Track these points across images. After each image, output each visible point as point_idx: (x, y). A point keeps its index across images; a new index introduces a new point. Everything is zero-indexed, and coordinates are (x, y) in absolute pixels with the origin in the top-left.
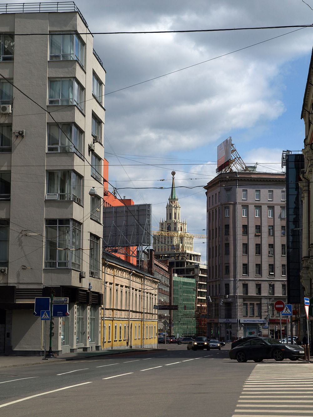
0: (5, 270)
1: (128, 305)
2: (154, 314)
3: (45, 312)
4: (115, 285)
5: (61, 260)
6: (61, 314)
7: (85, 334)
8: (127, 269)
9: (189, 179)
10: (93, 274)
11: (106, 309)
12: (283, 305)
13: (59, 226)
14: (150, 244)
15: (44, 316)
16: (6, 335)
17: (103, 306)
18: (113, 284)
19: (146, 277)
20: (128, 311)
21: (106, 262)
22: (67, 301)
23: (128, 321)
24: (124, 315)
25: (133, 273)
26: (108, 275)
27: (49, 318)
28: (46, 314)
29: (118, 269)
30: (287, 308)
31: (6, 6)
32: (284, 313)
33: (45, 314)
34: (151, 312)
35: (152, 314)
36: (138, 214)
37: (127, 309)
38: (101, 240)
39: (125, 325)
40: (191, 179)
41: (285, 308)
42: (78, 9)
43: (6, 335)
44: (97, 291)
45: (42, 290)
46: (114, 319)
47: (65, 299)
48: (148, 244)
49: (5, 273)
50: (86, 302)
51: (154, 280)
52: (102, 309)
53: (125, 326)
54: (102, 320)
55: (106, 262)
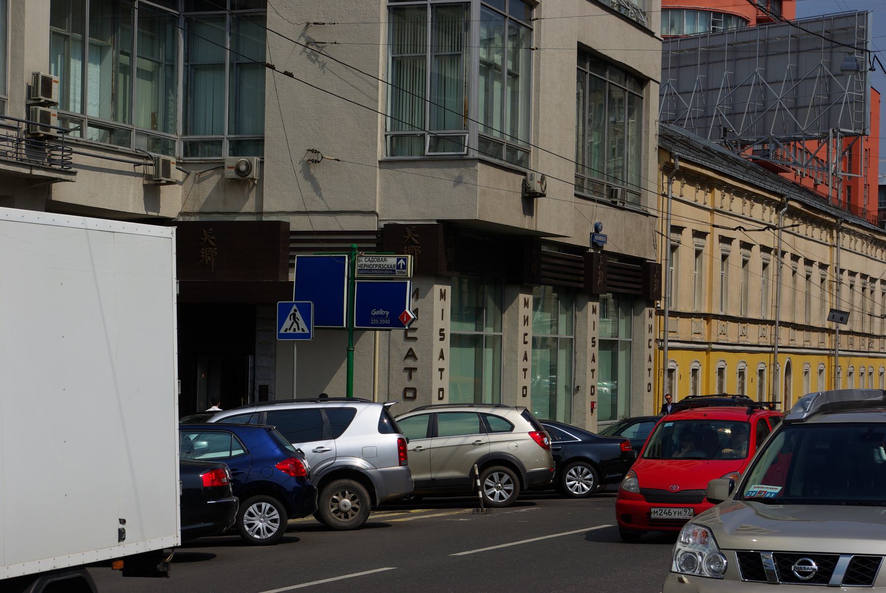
0: (249, 166)
1: (774, 304)
2: (878, 337)
3: (295, 307)
4: (716, 239)
7: (578, 395)
8: (767, 195)
10: (616, 197)
11: (674, 314)
14: (864, 130)
15: (288, 323)
16: (257, 394)
17: (661, 304)
18: (708, 237)
19: (843, 225)
20: (772, 323)
21: (673, 161)
22: (405, 267)
23: (772, 355)
24: (753, 334)
25: (790, 206)
26: (689, 207)
27: (307, 331)
28: (298, 315)
29: (729, 189)
32: (286, 330)
33: (294, 315)
34: (867, 331)
35: (871, 336)
37: (769, 318)
38: (654, 90)
39: (762, 366)
44: (633, 253)
45: (374, 237)
46: (714, 346)
47: (398, 260)
48: (858, 131)
49: (250, 176)
50: (640, 293)
51: (877, 236)
52: (660, 313)
53: (761, 372)
54: (661, 348)
55: (673, 161)
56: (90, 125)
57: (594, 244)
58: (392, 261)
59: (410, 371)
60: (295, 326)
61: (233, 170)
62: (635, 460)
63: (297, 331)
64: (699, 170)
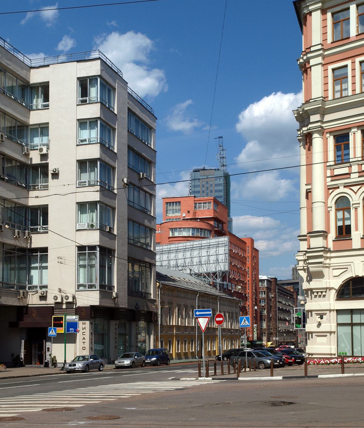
3: (53, 329)
5: (92, 282)
6: (73, 330)
9: (62, 185)
12: (222, 318)
13: (89, 253)
15: (51, 332)
16: (47, 350)
28: (53, 330)
30: (245, 320)
31: (44, 60)
36: (145, 235)
40: (64, 185)
41: (244, 320)
42: (314, 101)
43: (47, 350)
56: (5, 284)
57: (136, 308)
58: (74, 317)
59: (84, 339)
60: (245, 323)
61: (40, 294)
62: (251, 357)
63: (246, 325)
64: (340, 239)
